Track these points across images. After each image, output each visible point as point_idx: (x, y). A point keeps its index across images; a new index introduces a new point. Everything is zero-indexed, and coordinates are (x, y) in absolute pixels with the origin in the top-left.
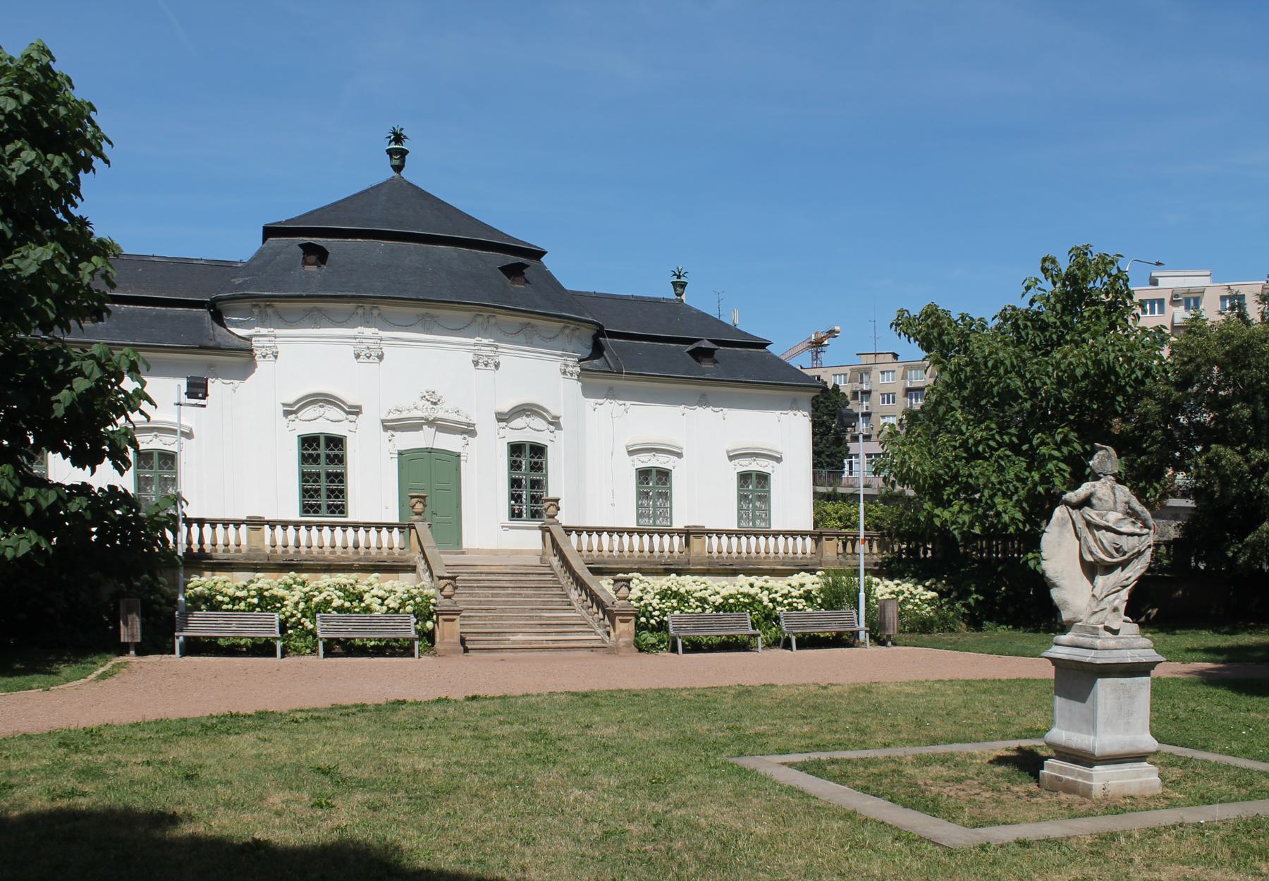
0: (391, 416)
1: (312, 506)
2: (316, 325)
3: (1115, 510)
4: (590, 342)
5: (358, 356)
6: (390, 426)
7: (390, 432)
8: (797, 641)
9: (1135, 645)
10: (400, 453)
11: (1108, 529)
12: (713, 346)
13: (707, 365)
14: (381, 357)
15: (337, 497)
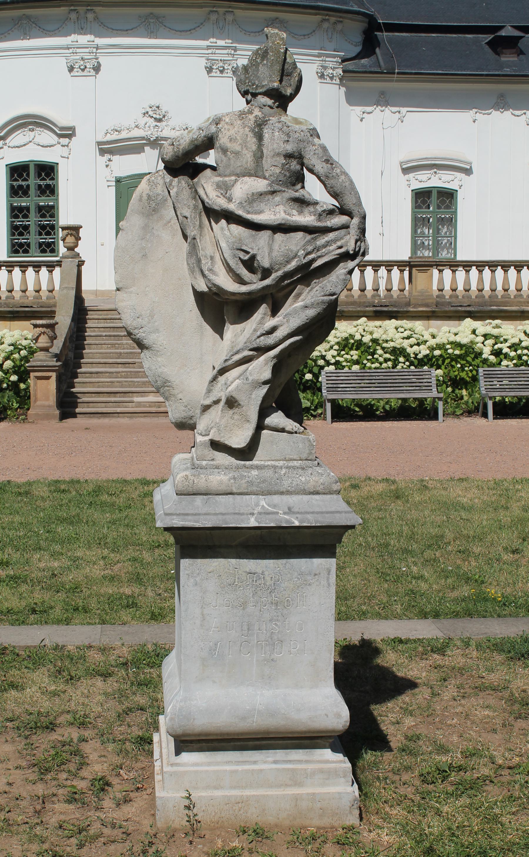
0: (109, 138)
1: (21, 245)
2: (26, 35)
3: (256, 172)
4: (359, 38)
5: (71, 69)
6: (108, 149)
7: (107, 156)
8: (495, 404)
9: (286, 484)
10: (118, 181)
11: (231, 218)
12: (517, 33)
13: (509, 58)
14: (97, 69)
15: (48, 234)
